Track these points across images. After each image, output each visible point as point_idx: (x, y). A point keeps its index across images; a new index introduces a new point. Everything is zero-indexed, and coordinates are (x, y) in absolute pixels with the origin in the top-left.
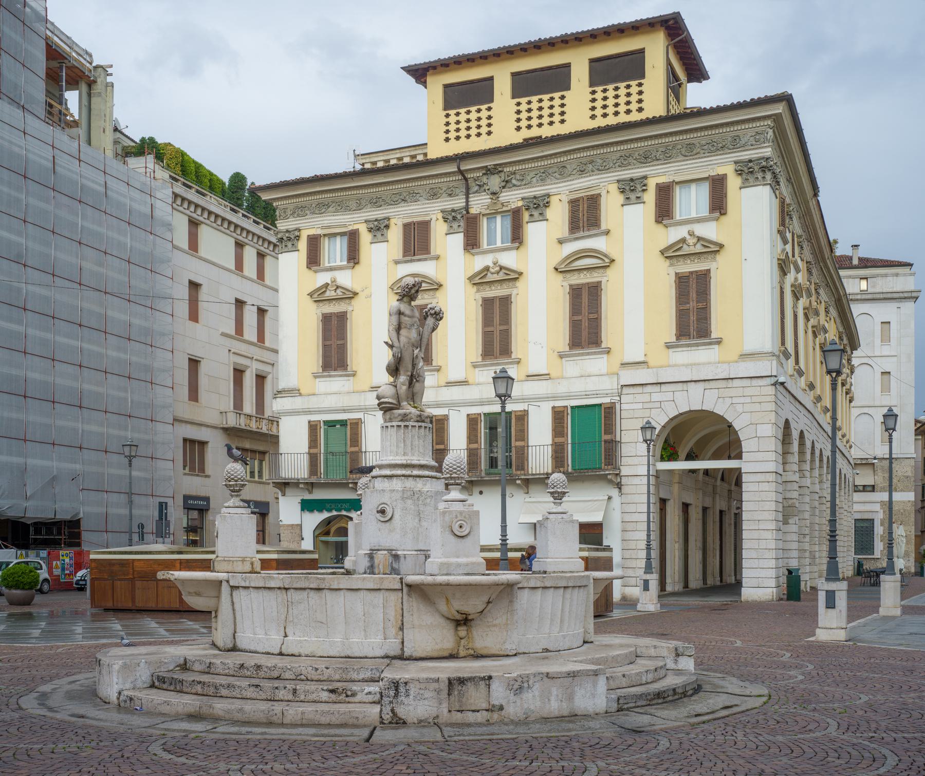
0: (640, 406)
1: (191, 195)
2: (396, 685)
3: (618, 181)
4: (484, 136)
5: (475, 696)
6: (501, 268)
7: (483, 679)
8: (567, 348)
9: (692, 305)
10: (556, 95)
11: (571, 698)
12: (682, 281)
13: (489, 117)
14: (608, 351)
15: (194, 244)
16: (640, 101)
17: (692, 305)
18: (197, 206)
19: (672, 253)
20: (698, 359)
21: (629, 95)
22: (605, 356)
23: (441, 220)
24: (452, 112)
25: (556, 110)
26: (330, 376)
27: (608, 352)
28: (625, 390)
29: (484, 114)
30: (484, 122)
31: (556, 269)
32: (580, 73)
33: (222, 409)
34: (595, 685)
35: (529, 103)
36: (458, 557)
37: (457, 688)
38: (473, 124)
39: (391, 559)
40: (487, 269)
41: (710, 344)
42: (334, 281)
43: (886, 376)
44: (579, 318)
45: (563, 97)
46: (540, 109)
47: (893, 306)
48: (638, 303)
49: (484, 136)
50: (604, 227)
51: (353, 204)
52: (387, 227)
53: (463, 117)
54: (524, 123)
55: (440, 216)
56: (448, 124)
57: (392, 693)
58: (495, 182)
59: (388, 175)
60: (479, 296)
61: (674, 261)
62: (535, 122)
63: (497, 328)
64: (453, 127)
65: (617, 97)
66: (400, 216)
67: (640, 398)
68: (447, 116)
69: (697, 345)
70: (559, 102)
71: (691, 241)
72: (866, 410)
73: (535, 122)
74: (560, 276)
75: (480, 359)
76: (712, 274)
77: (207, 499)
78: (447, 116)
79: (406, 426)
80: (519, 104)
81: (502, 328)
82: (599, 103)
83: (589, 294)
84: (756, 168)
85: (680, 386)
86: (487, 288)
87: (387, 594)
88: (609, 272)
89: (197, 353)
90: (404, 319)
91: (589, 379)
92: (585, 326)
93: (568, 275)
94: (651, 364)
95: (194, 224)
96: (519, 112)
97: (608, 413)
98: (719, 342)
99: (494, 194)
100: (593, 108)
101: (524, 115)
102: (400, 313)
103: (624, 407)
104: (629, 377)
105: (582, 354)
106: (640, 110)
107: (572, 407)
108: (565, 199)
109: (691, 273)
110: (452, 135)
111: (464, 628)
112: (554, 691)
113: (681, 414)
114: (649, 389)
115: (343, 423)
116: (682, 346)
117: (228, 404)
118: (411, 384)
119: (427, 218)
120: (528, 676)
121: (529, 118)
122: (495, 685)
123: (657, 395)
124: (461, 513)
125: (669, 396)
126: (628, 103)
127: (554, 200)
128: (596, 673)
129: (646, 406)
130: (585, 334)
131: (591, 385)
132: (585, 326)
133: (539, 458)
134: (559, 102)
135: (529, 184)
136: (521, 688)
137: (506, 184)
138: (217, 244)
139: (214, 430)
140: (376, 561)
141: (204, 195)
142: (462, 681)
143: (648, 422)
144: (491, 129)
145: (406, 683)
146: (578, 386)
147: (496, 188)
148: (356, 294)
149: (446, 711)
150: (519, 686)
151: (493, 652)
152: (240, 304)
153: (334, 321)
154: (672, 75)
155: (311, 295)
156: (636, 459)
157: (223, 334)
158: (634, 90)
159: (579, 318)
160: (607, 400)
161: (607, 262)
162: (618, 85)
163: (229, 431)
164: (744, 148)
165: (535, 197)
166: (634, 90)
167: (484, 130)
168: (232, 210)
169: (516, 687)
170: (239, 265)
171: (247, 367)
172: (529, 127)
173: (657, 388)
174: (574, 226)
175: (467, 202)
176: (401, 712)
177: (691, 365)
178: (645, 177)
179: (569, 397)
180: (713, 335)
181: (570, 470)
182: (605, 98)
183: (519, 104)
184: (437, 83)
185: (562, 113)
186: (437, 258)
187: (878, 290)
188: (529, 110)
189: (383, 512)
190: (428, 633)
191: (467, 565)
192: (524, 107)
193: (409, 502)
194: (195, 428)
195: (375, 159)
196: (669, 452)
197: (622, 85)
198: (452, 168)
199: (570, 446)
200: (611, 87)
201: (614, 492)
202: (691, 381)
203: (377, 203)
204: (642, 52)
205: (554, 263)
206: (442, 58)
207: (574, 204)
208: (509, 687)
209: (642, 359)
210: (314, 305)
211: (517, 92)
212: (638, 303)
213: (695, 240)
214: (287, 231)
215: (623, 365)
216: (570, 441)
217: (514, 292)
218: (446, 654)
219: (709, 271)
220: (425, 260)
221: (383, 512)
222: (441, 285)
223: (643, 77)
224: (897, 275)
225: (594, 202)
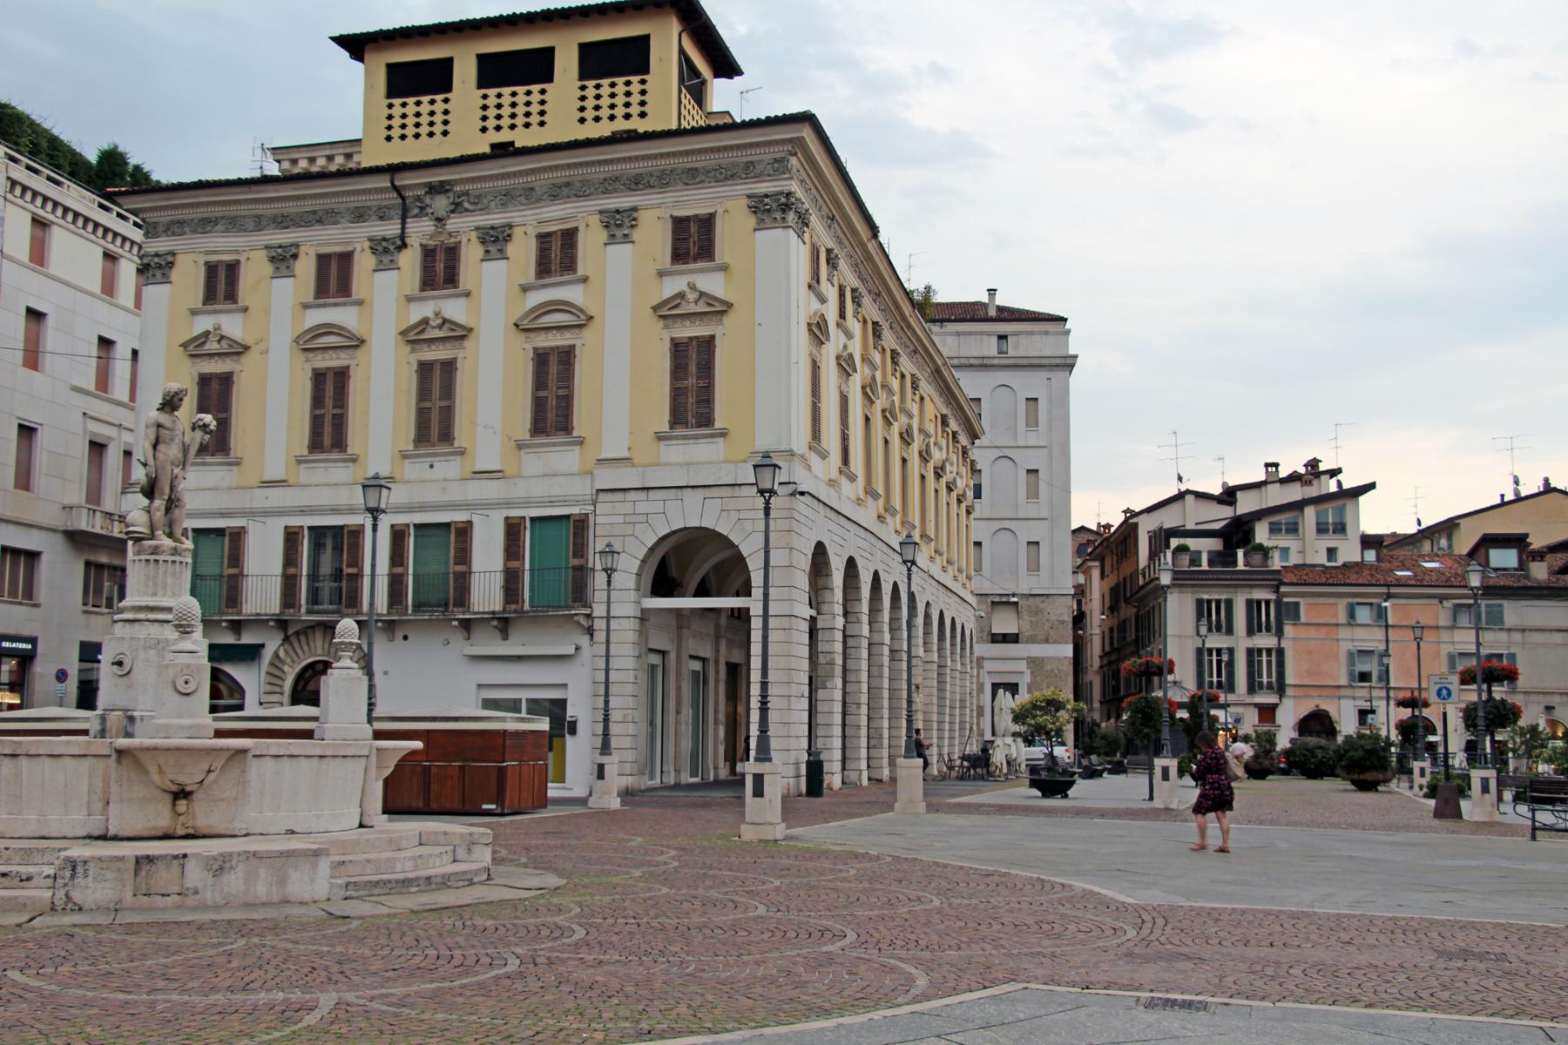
0: (620, 519)
1: (39, 183)
2: (73, 865)
3: (601, 212)
4: (438, 137)
5: (164, 877)
6: (445, 321)
7: (176, 857)
8: (527, 436)
9: (691, 381)
10: (536, 88)
11: (282, 882)
12: (679, 349)
13: (446, 112)
14: (581, 442)
15: (39, 255)
16: (643, 103)
17: (691, 381)
18: (46, 199)
19: (667, 311)
20: (696, 456)
21: (628, 94)
22: (577, 448)
23: (368, 251)
24: (397, 102)
25: (535, 108)
26: (205, 464)
27: (581, 443)
28: (602, 497)
29: (439, 107)
30: (438, 118)
31: (517, 325)
32: (567, 63)
33: (67, 502)
34: (315, 867)
35: (499, 96)
36: (181, 717)
37: (145, 867)
38: (425, 120)
39: (125, 722)
40: (425, 321)
41: (713, 436)
42: (218, 328)
43: (1032, 476)
44: (545, 394)
45: (543, 92)
46: (514, 105)
47: (1042, 375)
48: (622, 379)
49: (438, 137)
50: (581, 271)
51: (251, 224)
52: (295, 256)
53: (411, 109)
54: (491, 123)
55: (367, 244)
56: (390, 117)
57: (68, 874)
58: (441, 204)
59: (308, 181)
60: (414, 359)
61: (670, 321)
62: (506, 122)
63: (437, 403)
64: (397, 122)
65: (613, 95)
66: (315, 241)
67: (621, 508)
68: (390, 106)
69: (696, 437)
70: (539, 97)
71: (692, 296)
72: (1006, 524)
73: (506, 122)
74: (522, 336)
75: (411, 447)
76: (717, 342)
77: (33, 640)
78: (390, 106)
79: (157, 561)
80: (485, 97)
81: (444, 403)
82: (590, 103)
83: (560, 362)
84: (774, 205)
85: (672, 494)
86: (425, 347)
87: (94, 760)
88: (586, 332)
89: (32, 418)
90: (162, 431)
91: (552, 480)
92: (552, 409)
93: (532, 335)
94: (636, 461)
95: (39, 223)
96: (485, 108)
97: (579, 526)
98: (723, 434)
99: (439, 220)
100: (582, 109)
101: (492, 112)
102: (159, 426)
103: (600, 520)
104: (607, 478)
105: (547, 445)
106: (643, 115)
107: (533, 519)
108: (532, 232)
109: (691, 339)
110: (396, 132)
111: (184, 802)
112: (263, 873)
113: (674, 532)
114: (632, 496)
115: (220, 532)
116: (677, 437)
117: (77, 495)
118: (168, 510)
119: (350, 248)
120: (231, 854)
121: (499, 117)
122: (190, 865)
123: (643, 504)
124: (188, 666)
125: (659, 506)
126: (627, 105)
127: (518, 233)
128: (316, 854)
129: (628, 519)
130: (551, 416)
131: (557, 488)
132: (552, 409)
133: (486, 594)
134: (539, 97)
135: (485, 210)
136: (221, 868)
137: (456, 208)
138: (76, 255)
139: (51, 534)
140: (109, 724)
141: (58, 183)
142: (150, 859)
143: (609, 545)
144: (448, 128)
145: (85, 862)
146: (538, 490)
147: (442, 213)
148: (247, 348)
149: (129, 895)
150: (219, 866)
151: (205, 831)
152: (105, 343)
153: (215, 385)
154: (688, 71)
155: (185, 346)
156: (621, 596)
157: (76, 389)
158: (636, 88)
159: (545, 394)
160: (575, 510)
161: (583, 321)
162: (616, 80)
163: (76, 539)
164: (759, 177)
165: (492, 228)
166: (636, 88)
167: (438, 128)
168: (101, 206)
169: (215, 867)
170: (109, 287)
171: (110, 438)
172: (498, 128)
173: (642, 495)
174: (544, 268)
175: (403, 228)
176: (77, 896)
177: (688, 464)
178: (635, 209)
179: (527, 504)
180: (718, 425)
181: (527, 607)
182: (598, 97)
183: (485, 97)
184: (381, 60)
185: (542, 113)
186: (360, 303)
187: (1022, 354)
188: (499, 106)
189: (120, 664)
190: (140, 810)
191: (191, 727)
192: (492, 101)
193: (152, 652)
194: (21, 530)
195: (296, 156)
196: (663, 584)
197: (620, 81)
198: (383, 182)
199: (527, 574)
200: (605, 82)
201: (584, 640)
202: (694, 486)
203: (283, 222)
204: (645, 39)
205: (516, 315)
206: (347, 54)
207: (544, 239)
208: (208, 867)
209: (625, 454)
210: (188, 362)
211: (484, 81)
212: (622, 379)
213: (696, 295)
214: (157, 255)
215: (602, 461)
216: (527, 566)
217: (461, 354)
218: (159, 834)
219: (713, 337)
220: (344, 304)
221: (120, 664)
222: (363, 341)
223: (647, 71)
224: (1046, 333)
225: (569, 237)
